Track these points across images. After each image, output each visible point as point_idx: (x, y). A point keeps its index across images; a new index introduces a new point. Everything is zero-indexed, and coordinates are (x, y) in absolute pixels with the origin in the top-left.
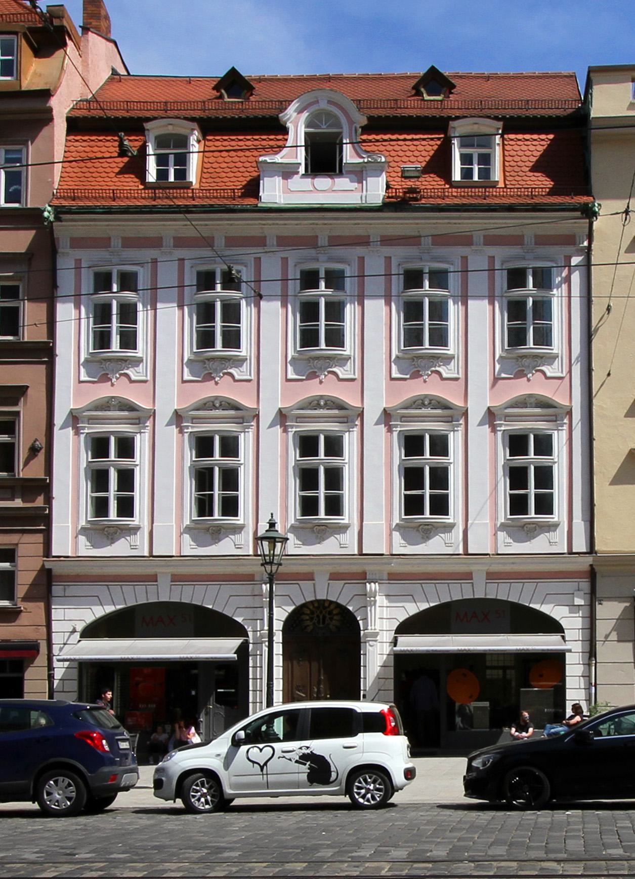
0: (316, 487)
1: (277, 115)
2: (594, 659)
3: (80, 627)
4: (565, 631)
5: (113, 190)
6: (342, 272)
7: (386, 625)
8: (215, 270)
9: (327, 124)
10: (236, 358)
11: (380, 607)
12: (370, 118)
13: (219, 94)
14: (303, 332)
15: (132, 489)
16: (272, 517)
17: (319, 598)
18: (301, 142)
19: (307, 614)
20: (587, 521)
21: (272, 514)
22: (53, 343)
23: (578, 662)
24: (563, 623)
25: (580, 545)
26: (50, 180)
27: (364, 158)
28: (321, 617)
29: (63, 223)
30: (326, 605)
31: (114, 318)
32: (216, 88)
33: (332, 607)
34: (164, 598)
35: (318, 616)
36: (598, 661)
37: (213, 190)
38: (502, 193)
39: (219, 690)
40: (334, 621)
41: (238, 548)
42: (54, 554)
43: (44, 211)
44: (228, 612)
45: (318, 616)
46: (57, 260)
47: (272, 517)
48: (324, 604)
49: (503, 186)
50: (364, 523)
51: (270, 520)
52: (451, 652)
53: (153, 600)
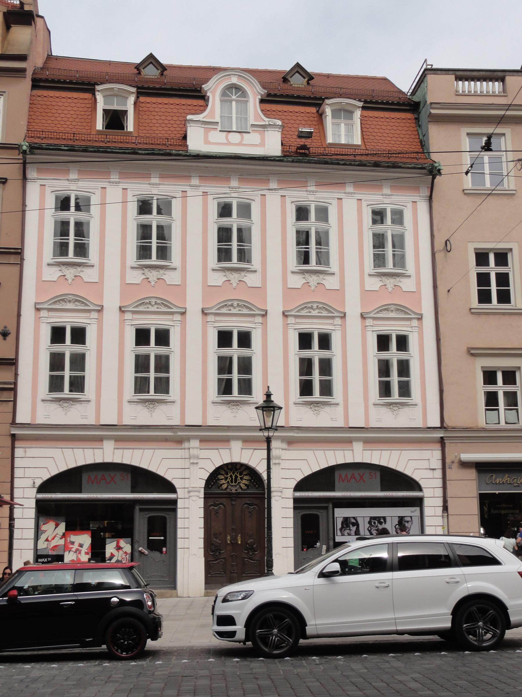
3: (38, 483)
4: (424, 490)
10: (243, 257)
12: (269, 95)
13: (138, 72)
19: (246, 475)
24: (422, 483)
25: (434, 421)
27: (265, 121)
30: (238, 467)
33: (243, 468)
35: (231, 476)
36: (449, 514)
39: (150, 538)
40: (244, 481)
42: (17, 422)
45: (231, 476)
46: (27, 185)
47: (268, 389)
48: (236, 466)
49: (365, 148)
51: (267, 392)
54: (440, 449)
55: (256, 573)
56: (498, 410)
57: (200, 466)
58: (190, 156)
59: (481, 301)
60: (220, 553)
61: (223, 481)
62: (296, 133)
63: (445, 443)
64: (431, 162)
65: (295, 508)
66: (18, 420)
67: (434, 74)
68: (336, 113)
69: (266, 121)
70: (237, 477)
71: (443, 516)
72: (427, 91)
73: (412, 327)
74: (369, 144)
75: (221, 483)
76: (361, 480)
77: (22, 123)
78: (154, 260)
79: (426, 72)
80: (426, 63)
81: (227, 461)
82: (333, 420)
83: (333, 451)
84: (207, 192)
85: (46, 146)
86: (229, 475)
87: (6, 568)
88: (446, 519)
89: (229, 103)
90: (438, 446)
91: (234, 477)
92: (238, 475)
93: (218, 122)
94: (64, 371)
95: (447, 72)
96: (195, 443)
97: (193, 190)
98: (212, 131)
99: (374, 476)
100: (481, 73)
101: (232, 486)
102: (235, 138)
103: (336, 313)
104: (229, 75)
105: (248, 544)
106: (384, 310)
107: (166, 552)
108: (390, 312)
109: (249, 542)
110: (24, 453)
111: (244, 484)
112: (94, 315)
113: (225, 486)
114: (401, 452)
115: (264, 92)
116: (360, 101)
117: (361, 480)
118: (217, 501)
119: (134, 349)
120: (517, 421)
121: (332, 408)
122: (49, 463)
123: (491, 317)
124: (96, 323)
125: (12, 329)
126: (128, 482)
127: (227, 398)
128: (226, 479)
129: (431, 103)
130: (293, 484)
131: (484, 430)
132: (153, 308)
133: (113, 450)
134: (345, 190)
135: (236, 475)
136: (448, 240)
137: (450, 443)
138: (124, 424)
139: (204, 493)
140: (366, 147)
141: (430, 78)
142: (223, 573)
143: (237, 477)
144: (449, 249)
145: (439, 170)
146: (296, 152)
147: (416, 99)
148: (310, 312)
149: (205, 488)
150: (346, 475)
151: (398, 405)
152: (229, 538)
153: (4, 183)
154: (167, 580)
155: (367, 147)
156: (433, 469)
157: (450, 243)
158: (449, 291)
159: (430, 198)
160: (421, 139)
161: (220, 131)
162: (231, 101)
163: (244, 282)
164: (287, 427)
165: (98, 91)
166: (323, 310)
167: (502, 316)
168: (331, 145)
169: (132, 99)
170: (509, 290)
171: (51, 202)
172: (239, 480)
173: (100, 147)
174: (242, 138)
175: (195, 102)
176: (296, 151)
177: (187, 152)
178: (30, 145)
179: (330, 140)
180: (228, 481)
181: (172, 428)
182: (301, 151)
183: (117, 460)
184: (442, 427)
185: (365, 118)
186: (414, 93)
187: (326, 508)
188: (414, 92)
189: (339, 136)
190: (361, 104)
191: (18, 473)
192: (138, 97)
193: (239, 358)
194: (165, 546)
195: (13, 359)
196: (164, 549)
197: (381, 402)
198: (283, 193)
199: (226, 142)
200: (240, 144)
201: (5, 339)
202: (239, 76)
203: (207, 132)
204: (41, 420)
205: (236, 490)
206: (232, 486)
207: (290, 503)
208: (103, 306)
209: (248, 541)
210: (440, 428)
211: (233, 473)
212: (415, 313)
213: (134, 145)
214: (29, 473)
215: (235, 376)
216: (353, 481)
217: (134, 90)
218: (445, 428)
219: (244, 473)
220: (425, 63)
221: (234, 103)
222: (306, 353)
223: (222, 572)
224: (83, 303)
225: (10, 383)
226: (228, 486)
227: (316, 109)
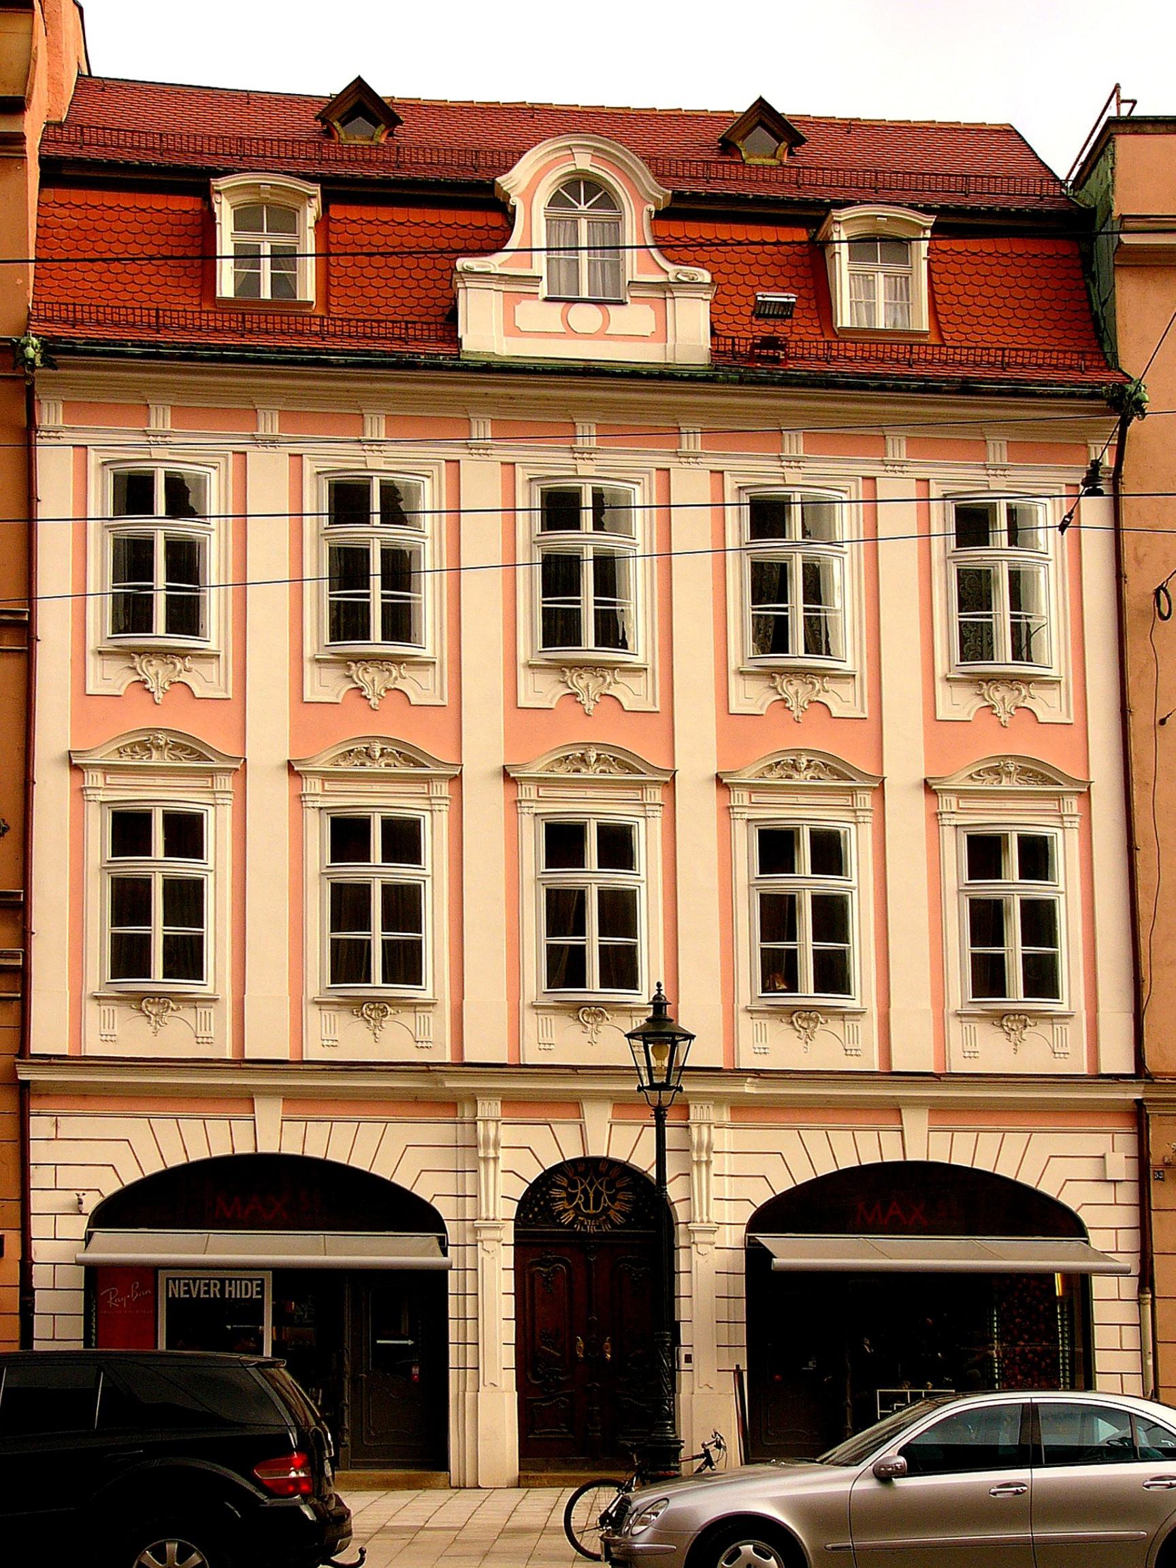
0: (145, 918)
1: (494, 181)
2: (1148, 1289)
3: (91, 1203)
8: (153, 472)
9: (577, 204)
11: (715, 1175)
12: (678, 197)
14: (336, 608)
15: (1052, 942)
17: (593, 1153)
18: (539, 239)
19: (622, 1189)
20: (1129, 1013)
22: (30, 614)
23: (52, 1287)
24: (1085, 1216)
25: (1118, 1059)
26: (19, 281)
29: (59, 371)
31: (376, 582)
32: (323, 118)
34: (268, 1146)
35: (585, 1192)
37: (358, 321)
38: (922, 356)
39: (378, 1342)
41: (420, 1045)
43: (25, 346)
44: (1048, 1188)
51: (655, 998)
52: (325, 1267)
53: (245, 1148)
58: (466, 369)
62: (748, 311)
64: (1119, 378)
67: (1136, 133)
68: (863, 245)
70: (602, 1193)
71: (1140, 1302)
72: (1113, 181)
74: (952, 329)
78: (376, 643)
79: (1113, 129)
80: (1118, 96)
81: (573, 1152)
85: (85, 344)
87: (1065, 517)
91: (591, 1195)
93: (541, 278)
96: (489, 1109)
98: (524, 302)
101: (588, 1216)
102: (585, 317)
111: (618, 1211)
113: (567, 1218)
114: (1031, 1136)
115: (661, 195)
127: (573, 995)
129: (1123, 218)
130: (748, 1212)
133: (280, 1122)
135: (597, 1188)
136: (1161, 588)
137: (1160, 1115)
139: (515, 1232)
140: (941, 337)
141: (1124, 144)
144: (1165, 610)
145: (1139, 402)
146: (752, 358)
147: (1089, 196)
148: (789, 777)
155: (946, 336)
157: (1168, 596)
160: (1097, 313)
161: (546, 300)
165: (219, 192)
166: (823, 772)
169: (311, 213)
171: (100, 498)
172: (605, 1202)
173: (227, 348)
174: (607, 320)
175: (478, 218)
176: (752, 351)
177: (459, 359)
178: (42, 343)
179: (845, 318)
181: (429, 1071)
182: (764, 353)
184: (1141, 1072)
185: (942, 257)
186: (1081, 181)
188: (1082, 179)
189: (871, 307)
190: (930, 220)
191: (38, 1178)
192: (325, 207)
193: (601, 893)
197: (976, 1010)
200: (602, 335)
202: (596, 149)
204: (94, 1047)
206: (588, 1216)
208: (245, 759)
211: (591, 1184)
212: (1072, 781)
213: (316, 339)
214: (68, 1177)
215: (593, 941)
217: (316, 189)
218: (1148, 1076)
220: (1115, 95)
223: (563, 1427)
224: (193, 751)
227: (808, 233)
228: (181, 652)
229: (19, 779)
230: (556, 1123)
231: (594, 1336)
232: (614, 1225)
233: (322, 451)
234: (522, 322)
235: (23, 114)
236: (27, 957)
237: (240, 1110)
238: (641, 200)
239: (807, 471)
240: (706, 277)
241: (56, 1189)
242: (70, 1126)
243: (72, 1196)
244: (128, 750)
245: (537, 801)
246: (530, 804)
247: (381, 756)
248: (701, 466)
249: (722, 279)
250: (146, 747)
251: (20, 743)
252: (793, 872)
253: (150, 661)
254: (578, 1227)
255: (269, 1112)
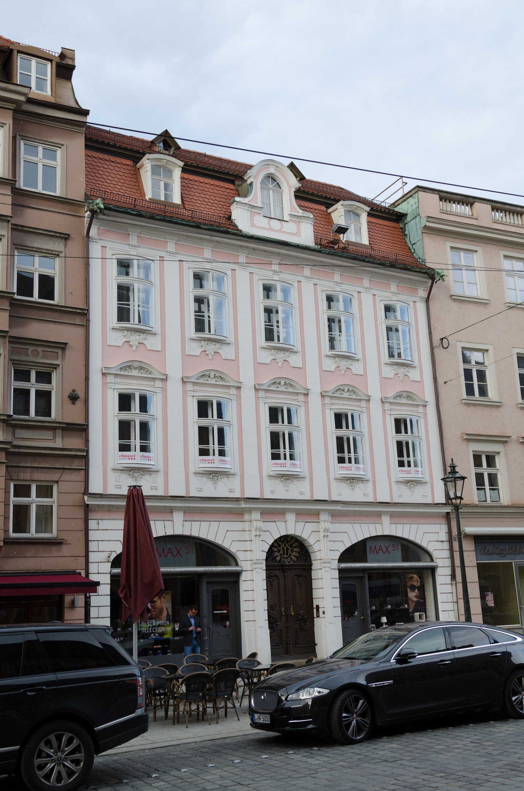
5: (135, 199)
6: (275, 286)
7: (103, 556)
16: (452, 461)
19: (295, 547)
21: (452, 460)
28: (285, 549)
33: (293, 541)
35: (283, 548)
36: (457, 582)
39: (215, 612)
40: (294, 553)
41: (301, 493)
45: (283, 548)
47: (452, 461)
50: (43, 480)
54: (447, 523)
55: (308, 644)
56: (484, 489)
57: (262, 538)
59: (468, 394)
60: (277, 625)
61: (277, 554)
63: (450, 518)
65: (340, 578)
66: (91, 491)
67: (424, 191)
69: (300, 212)
70: (289, 549)
73: (419, 413)
75: (275, 555)
76: (178, 554)
77: (82, 180)
82: (120, 487)
83: (359, 524)
84: (163, 257)
86: (282, 547)
88: (454, 587)
89: (267, 191)
90: (444, 521)
91: (285, 550)
92: (289, 548)
94: (130, 440)
95: (433, 192)
97: (242, 269)
99: (396, 548)
100: (458, 197)
102: (275, 224)
103: (232, 383)
104: (268, 165)
105: (300, 615)
106: (125, 367)
107: (229, 626)
108: (133, 369)
109: (301, 613)
110: (97, 526)
112: (158, 384)
113: (278, 558)
116: (369, 206)
117: (178, 554)
118: (271, 573)
119: (197, 421)
120: (498, 500)
121: (364, 484)
122: (344, 537)
123: (478, 408)
124: (161, 392)
125: (82, 395)
126: (192, 556)
128: (279, 551)
130: (337, 555)
131: (476, 506)
132: (212, 381)
134: (129, 242)
135: (287, 547)
138: (191, 496)
142: (280, 645)
143: (289, 549)
144: (445, 346)
149: (266, 560)
150: (163, 550)
151: (414, 483)
152: (283, 609)
153: (66, 239)
154: (232, 654)
156: (442, 541)
158: (445, 383)
159: (427, 300)
162: (269, 190)
163: (287, 362)
164: (242, 498)
167: (484, 408)
168: (152, 201)
170: (478, 382)
171: (113, 267)
180: (281, 553)
183: (187, 532)
187: (361, 578)
191: (92, 546)
194: (229, 621)
195: (84, 425)
196: (228, 623)
198: (104, 244)
199: (269, 227)
200: (280, 231)
201: (74, 403)
203: (252, 215)
205: (289, 562)
207: (336, 574)
209: (299, 612)
210: (445, 504)
214: (103, 546)
216: (170, 555)
219: (294, 545)
221: (271, 191)
222: (125, 416)
225: (82, 451)
226: (281, 558)
228: (144, 331)
229: (83, 377)
230: (278, 521)
231: (288, 606)
232: (294, 561)
233: (264, 273)
234: (257, 223)
235: (87, 116)
236: (87, 451)
237: (167, 517)
238: (289, 186)
239: (281, 276)
240: (312, 216)
241: (98, 551)
242: (104, 524)
243: (107, 554)
244: (124, 369)
245: (266, 398)
246: (263, 399)
247: (348, 391)
248: (311, 282)
249: (315, 218)
250: (400, 396)
251: (83, 363)
252: (278, 423)
253: (131, 334)
254: (282, 563)
255: (178, 517)
